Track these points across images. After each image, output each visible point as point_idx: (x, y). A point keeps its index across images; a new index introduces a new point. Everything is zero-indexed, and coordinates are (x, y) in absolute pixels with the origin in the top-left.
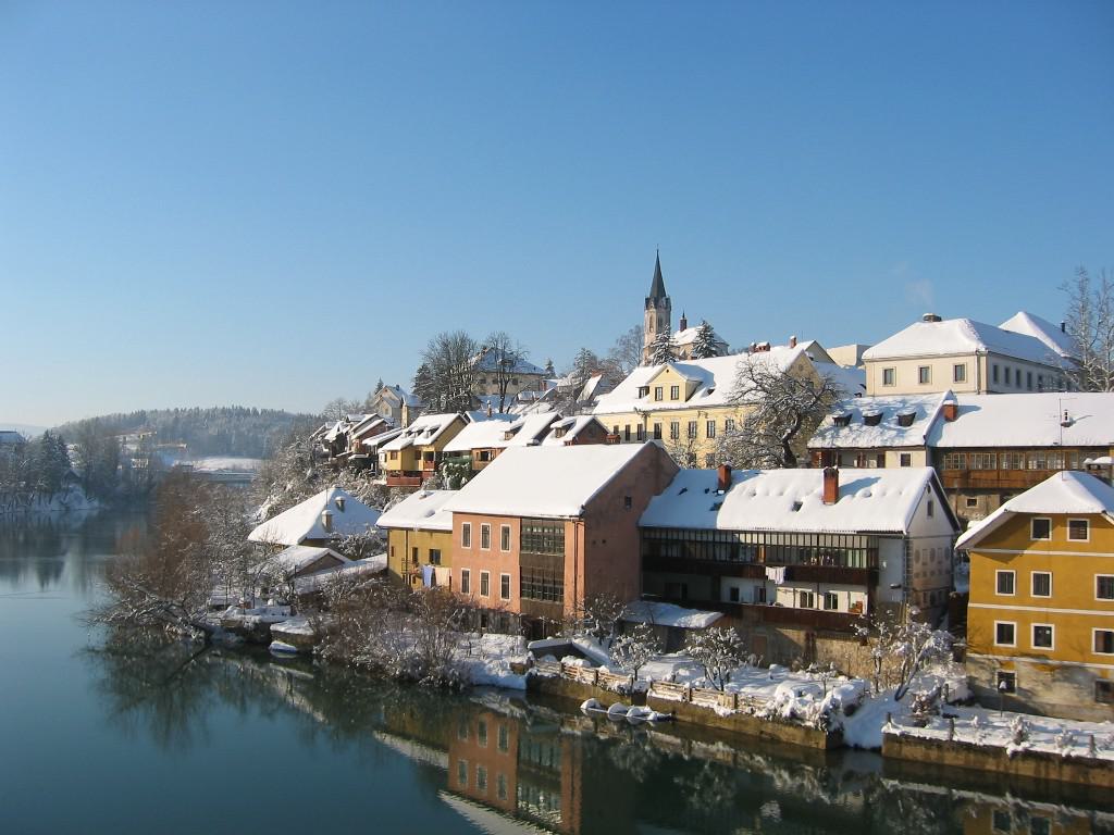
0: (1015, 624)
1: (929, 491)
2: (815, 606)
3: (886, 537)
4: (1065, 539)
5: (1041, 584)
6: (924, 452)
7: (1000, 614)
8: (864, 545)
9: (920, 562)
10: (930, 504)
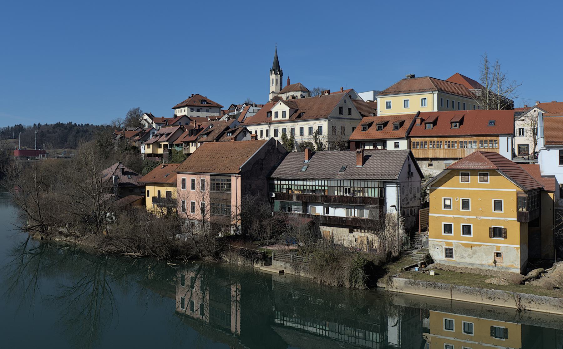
0: (453, 224)
1: (409, 160)
2: (353, 215)
3: (388, 182)
4: (478, 182)
5: (465, 205)
6: (406, 141)
7: (445, 219)
8: (377, 186)
9: (405, 194)
10: (409, 166)
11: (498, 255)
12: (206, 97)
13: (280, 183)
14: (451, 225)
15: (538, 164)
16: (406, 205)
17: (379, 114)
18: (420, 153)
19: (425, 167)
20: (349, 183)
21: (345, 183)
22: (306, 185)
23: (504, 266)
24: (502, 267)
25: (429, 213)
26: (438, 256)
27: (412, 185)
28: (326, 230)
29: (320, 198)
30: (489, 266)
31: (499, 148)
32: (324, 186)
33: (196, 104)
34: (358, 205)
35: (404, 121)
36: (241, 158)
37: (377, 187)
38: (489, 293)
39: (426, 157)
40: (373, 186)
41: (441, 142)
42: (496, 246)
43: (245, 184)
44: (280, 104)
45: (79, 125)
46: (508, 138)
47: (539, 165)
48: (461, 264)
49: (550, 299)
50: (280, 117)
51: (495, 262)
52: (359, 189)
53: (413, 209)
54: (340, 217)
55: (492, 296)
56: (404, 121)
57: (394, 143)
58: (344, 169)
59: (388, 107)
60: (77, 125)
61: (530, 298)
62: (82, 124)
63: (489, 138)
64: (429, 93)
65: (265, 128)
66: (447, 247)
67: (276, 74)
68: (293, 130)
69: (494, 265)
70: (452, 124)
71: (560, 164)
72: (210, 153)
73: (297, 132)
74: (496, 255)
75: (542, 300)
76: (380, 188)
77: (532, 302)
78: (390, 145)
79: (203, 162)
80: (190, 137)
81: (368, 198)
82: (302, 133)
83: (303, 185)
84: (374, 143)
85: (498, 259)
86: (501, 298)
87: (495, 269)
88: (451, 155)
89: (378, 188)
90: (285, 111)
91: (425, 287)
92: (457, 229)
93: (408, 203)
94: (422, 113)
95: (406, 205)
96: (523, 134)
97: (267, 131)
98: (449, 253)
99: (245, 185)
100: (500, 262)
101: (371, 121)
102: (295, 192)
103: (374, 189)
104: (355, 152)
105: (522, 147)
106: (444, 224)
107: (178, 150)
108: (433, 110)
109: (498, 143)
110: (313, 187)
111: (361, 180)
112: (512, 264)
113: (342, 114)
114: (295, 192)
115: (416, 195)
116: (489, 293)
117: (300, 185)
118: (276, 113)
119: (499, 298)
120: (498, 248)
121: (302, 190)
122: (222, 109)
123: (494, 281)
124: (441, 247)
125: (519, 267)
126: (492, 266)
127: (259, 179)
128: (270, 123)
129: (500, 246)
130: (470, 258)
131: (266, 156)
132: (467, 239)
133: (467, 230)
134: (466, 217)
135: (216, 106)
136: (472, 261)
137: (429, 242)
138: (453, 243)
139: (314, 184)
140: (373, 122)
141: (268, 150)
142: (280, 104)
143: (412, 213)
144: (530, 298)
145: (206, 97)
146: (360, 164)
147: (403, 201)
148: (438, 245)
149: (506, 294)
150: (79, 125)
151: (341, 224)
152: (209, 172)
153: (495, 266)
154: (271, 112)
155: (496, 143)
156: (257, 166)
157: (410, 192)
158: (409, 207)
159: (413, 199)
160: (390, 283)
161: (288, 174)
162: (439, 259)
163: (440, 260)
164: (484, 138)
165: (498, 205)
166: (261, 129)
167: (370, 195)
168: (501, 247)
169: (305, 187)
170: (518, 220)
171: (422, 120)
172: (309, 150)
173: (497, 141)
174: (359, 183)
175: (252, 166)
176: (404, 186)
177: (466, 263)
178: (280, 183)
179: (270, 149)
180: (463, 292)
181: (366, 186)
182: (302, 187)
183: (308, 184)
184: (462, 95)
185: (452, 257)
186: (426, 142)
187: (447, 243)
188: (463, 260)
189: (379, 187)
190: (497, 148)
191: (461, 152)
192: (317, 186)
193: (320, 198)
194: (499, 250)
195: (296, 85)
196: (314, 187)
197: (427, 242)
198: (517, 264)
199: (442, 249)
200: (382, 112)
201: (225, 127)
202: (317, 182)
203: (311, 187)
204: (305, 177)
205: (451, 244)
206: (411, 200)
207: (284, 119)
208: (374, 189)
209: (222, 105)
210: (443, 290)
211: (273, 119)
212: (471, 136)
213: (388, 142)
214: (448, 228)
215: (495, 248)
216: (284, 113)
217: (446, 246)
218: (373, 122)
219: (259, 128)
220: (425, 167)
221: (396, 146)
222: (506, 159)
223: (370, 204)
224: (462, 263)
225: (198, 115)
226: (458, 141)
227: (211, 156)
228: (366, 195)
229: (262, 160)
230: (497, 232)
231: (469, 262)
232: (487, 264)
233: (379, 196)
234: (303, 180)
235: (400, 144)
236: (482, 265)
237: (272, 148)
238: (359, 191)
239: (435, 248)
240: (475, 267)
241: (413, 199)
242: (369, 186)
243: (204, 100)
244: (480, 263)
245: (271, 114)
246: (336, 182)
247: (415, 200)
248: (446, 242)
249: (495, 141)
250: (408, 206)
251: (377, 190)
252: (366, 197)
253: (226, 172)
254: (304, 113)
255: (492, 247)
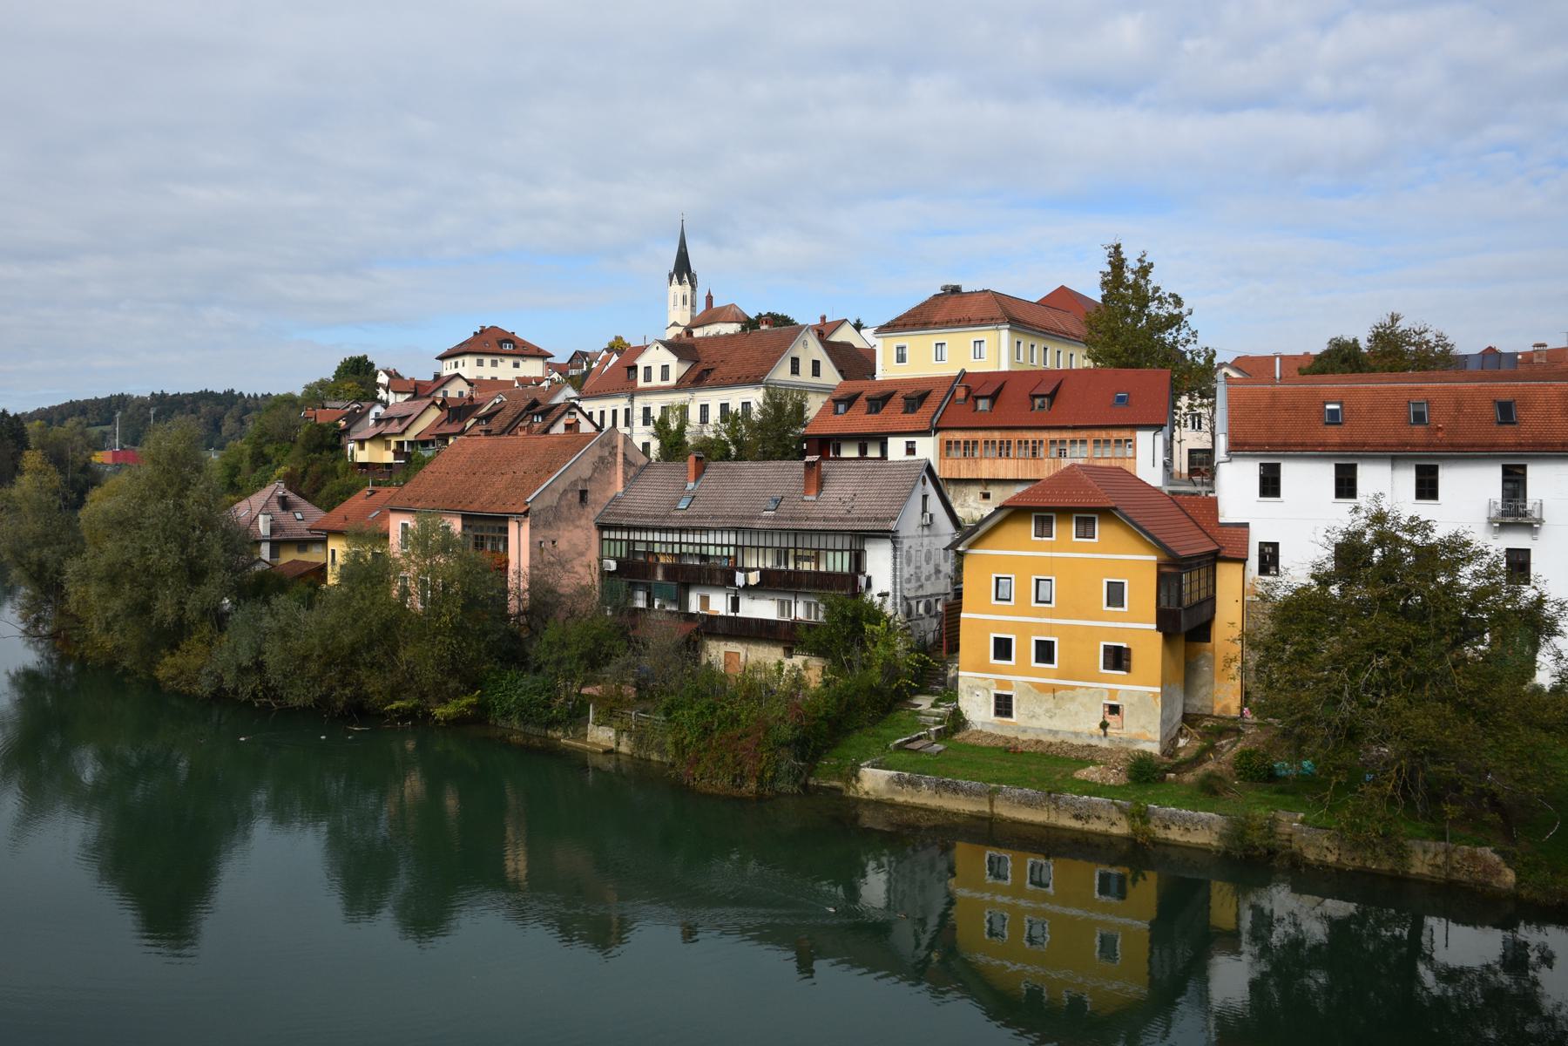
8: (847, 546)
9: (912, 566)
11: (1114, 709)
12: (513, 333)
13: (626, 538)
14: (1010, 640)
15: (1216, 495)
16: (916, 591)
17: (880, 375)
18: (962, 467)
19: (973, 501)
20: (784, 538)
21: (776, 539)
22: (687, 543)
23: (1125, 736)
24: (1120, 738)
25: (960, 612)
26: (977, 709)
27: (930, 543)
28: (717, 652)
29: (718, 575)
30: (1092, 736)
31: (1135, 458)
32: (728, 546)
33: (490, 350)
34: (805, 590)
35: (930, 392)
36: (535, 475)
37: (848, 548)
38: (1078, 805)
39: (975, 477)
40: (839, 546)
41: (1009, 443)
42: (1109, 690)
43: (541, 539)
44: (657, 348)
45: (249, 395)
46: (1154, 434)
47: (1216, 498)
48: (1029, 731)
49: (1213, 819)
50: (656, 380)
51: (1104, 725)
52: (807, 553)
53: (933, 600)
54: (762, 620)
55: (1084, 812)
56: (930, 392)
57: (905, 443)
58: (778, 502)
59: (901, 358)
60: (246, 396)
61: (1167, 817)
62: (256, 395)
63: (1116, 434)
64: (991, 327)
65: (621, 404)
66: (999, 692)
67: (681, 282)
68: (684, 410)
69: (1102, 733)
70: (1033, 401)
71: (1261, 496)
72: (468, 464)
73: (694, 415)
74: (1107, 709)
75: (1195, 820)
76: (855, 550)
77: (1172, 827)
78: (896, 448)
79: (448, 486)
80: (450, 426)
81: (827, 574)
82: (704, 419)
83: (681, 543)
84: (863, 441)
85: (1112, 719)
86: (1103, 816)
87: (1105, 744)
88: (1031, 472)
89: (850, 550)
90: (668, 366)
91: (933, 792)
92: (1023, 649)
93: (921, 586)
94: (969, 373)
95: (916, 591)
96: (1200, 427)
97: (627, 411)
98: (1004, 706)
99: (541, 542)
100: (1116, 726)
101: (857, 390)
102: (662, 560)
103: (840, 553)
104: (800, 464)
105: (1198, 456)
106: (996, 639)
107: (426, 455)
108: (999, 367)
109: (1134, 447)
110: (683, 546)
111: (812, 532)
112: (1143, 730)
113: (818, 375)
114: (662, 560)
115: (941, 568)
116: (1078, 805)
117: (673, 543)
118: (648, 369)
119: (1099, 818)
120: (1113, 693)
121: (676, 554)
122: (549, 360)
123: (1091, 773)
124: (985, 691)
125: (1158, 737)
126: (1099, 737)
127: (578, 527)
128: (633, 393)
129: (1118, 690)
130: (1051, 717)
131: (594, 471)
132: (1045, 674)
133: (1045, 652)
134: (1043, 624)
135: (536, 353)
136: (1055, 725)
137: (960, 681)
138: (1013, 683)
139: (704, 540)
140: (861, 393)
141: (600, 457)
142: (657, 348)
143: (930, 610)
144: (1167, 817)
145: (513, 333)
146: (812, 493)
147: (909, 581)
148: (978, 687)
149: (1114, 807)
150: (249, 395)
151: (763, 635)
152: (459, 508)
153: (1105, 735)
154: (635, 367)
155: (1130, 446)
156: (573, 497)
157: (907, 563)
158: (922, 597)
159: (933, 578)
160: (854, 782)
161: (647, 516)
162: (980, 720)
163: (983, 723)
164: (1103, 435)
165: (1115, 595)
166: (614, 408)
167: (831, 569)
168: (1119, 693)
169: (684, 549)
170: (1158, 629)
171: (968, 390)
172: (697, 458)
173: (1131, 440)
174: (807, 539)
175: (558, 496)
176: (910, 547)
177: (1041, 729)
178: (626, 538)
179: (607, 454)
180: (1019, 802)
181: (822, 546)
182: (677, 547)
183: (691, 540)
184: (1066, 334)
185: (1009, 714)
186: (975, 443)
187: (1000, 683)
188: (1035, 723)
189: (853, 548)
190: (1130, 458)
191: (1052, 467)
192: (711, 545)
193: (718, 575)
194: (1115, 700)
195: (726, 306)
196: (704, 548)
197: (956, 679)
198: (1153, 731)
199: (989, 697)
200: (886, 370)
201: (530, 401)
202: (711, 536)
203: (697, 548)
204: (685, 523)
205: (1008, 685)
206: (928, 578)
207: (665, 383)
208: (840, 553)
209: (550, 351)
210: (973, 797)
211: (641, 383)
212: (1075, 428)
213: (890, 440)
214: (1003, 649)
215: (1107, 694)
216: (665, 369)
217: (997, 689)
218: (861, 393)
219: (608, 405)
220: (973, 501)
221: (911, 450)
222: (1144, 482)
223: (831, 590)
224: (1033, 728)
225: (494, 376)
226: (1046, 440)
227: (468, 471)
228: (822, 568)
229: (585, 480)
230: (1118, 658)
231: (1047, 727)
232: (1087, 732)
233: (853, 571)
234: (681, 530)
235: (917, 447)
236: (1076, 734)
237: (610, 453)
238: (808, 559)
239: (973, 693)
240: (1058, 740)
241: (933, 578)
242: (830, 546)
243: (509, 339)
244: (1072, 729)
245: (636, 372)
246: (755, 538)
247: (938, 578)
248: (997, 680)
249: (1127, 441)
250: (920, 593)
251: (847, 555)
252: (822, 573)
253: (497, 509)
254: (712, 369)
255: (1101, 692)
